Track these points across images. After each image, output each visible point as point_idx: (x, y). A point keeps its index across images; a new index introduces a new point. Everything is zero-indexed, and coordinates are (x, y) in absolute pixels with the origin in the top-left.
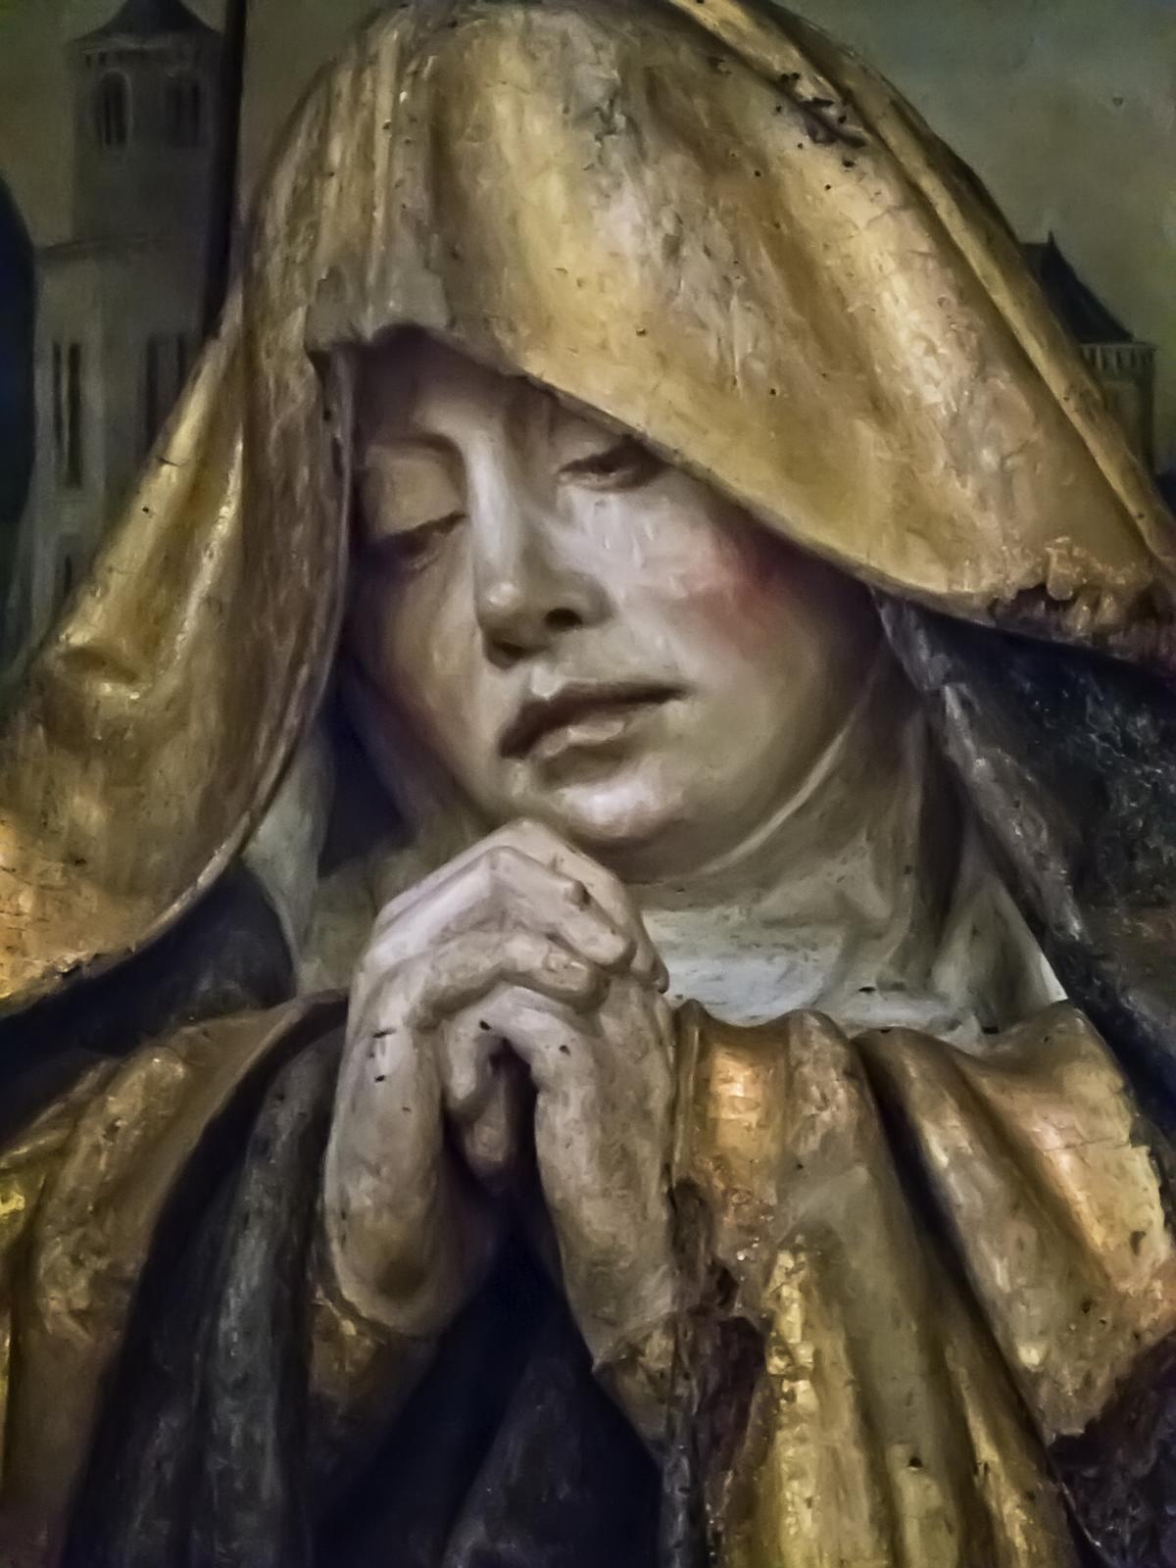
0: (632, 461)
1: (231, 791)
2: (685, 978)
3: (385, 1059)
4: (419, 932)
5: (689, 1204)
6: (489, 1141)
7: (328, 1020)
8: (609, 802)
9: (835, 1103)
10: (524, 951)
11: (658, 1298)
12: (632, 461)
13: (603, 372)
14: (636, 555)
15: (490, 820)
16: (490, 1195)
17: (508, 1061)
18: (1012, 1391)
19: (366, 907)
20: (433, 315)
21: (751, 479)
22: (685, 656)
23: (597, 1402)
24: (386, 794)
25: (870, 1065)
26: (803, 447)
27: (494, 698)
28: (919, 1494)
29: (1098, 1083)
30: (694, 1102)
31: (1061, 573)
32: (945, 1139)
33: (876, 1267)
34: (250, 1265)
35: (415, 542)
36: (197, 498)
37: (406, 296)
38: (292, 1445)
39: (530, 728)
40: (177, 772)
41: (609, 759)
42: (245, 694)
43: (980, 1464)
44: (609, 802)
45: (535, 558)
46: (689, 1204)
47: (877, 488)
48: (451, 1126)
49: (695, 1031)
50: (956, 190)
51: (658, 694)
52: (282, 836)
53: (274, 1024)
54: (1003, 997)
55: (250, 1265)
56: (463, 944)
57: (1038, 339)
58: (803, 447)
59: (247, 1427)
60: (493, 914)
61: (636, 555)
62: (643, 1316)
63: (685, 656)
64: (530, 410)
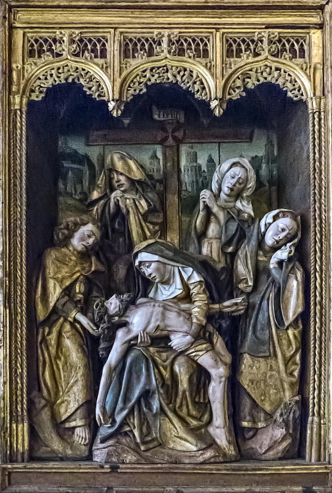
0: (122, 174)
1: (105, 190)
2: (125, 196)
3: (112, 201)
4: (113, 195)
5: (126, 206)
6: (117, 203)
7: (110, 199)
8: (122, 189)
9: (132, 201)
10: (118, 195)
11: (125, 210)
12: (122, 174)
13: (120, 170)
14: (122, 179)
15: (116, 190)
16: (117, 204)
17: (118, 200)
18: (140, 213)
19: (111, 194)
20: (112, 168)
21: (127, 174)
22: (125, 183)
23: (123, 214)
24: (112, 189)
25: (134, 200)
26: (130, 173)
27: (116, 184)
28: (136, 217)
29: (144, 200)
30: (126, 202)
31: (141, 178)
32: (137, 203)
33: (134, 207)
34: (107, 210)
35: (112, 178)
36: (103, 176)
37: (110, 167)
38: (109, 216)
39: (118, 186)
40: (103, 189)
41: (122, 187)
42: (105, 184)
43: (122, 301)
44: (122, 189)
45: (117, 179)
46: (126, 206)
47: (133, 175)
48: (115, 203)
49: (126, 198)
50: (136, 161)
51: (124, 184)
52: (108, 191)
53: (230, 485)
54: (140, 197)
55: (107, 210)
56: (116, 194)
57: (133, 236)
58: (130, 173)
59: (107, 215)
60: (117, 193)
61: (122, 178)
62: (124, 211)
63: (125, 183)
64: (117, 172)
